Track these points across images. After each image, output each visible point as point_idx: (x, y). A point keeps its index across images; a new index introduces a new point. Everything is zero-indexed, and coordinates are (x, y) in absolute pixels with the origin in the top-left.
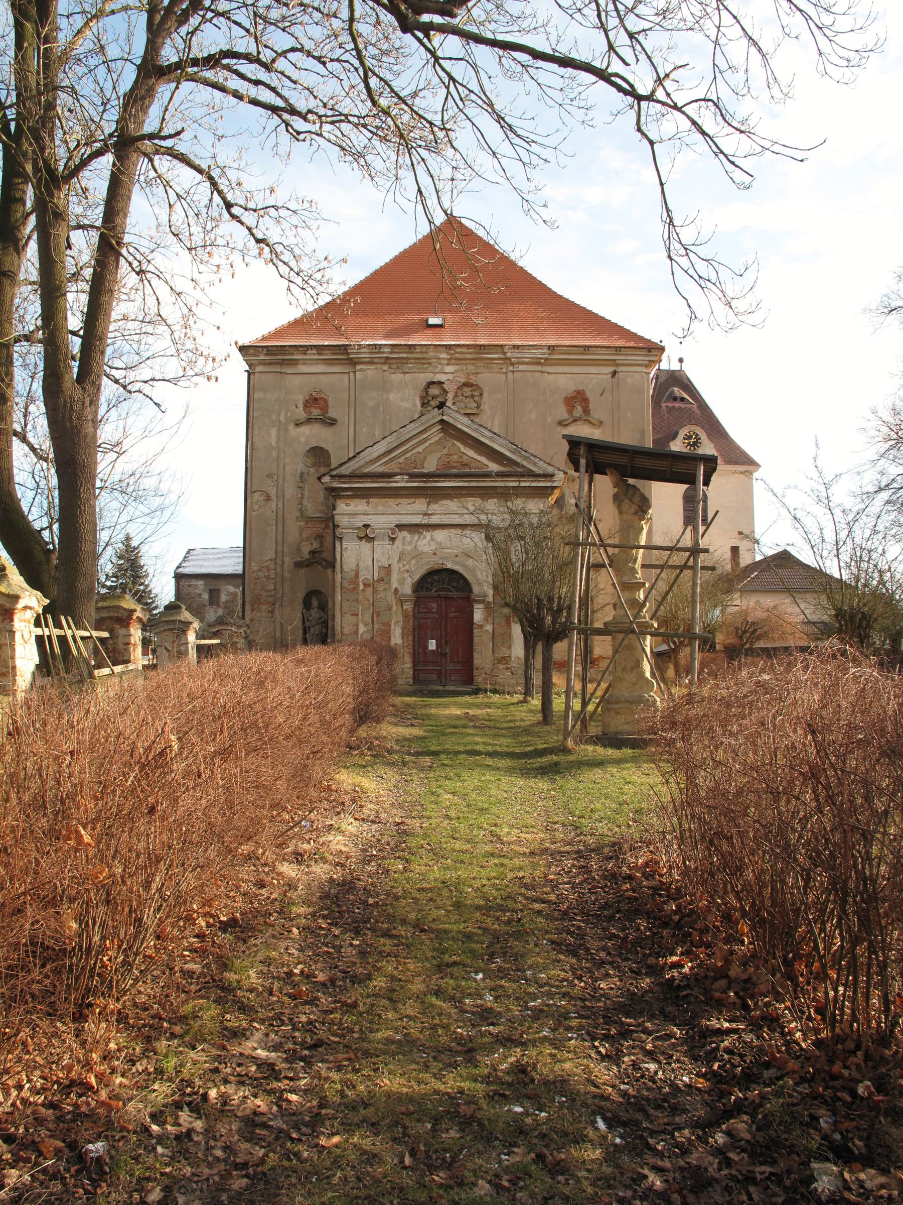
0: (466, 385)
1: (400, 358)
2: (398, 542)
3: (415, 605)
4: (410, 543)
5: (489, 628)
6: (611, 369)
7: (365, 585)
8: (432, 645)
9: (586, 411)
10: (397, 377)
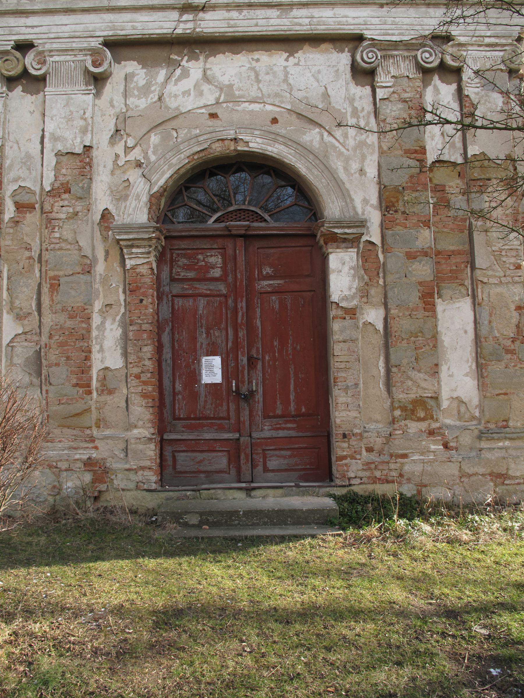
2: (112, 89)
3: (161, 259)
4: (145, 90)
5: (374, 316)
7: (19, 207)
8: (212, 370)
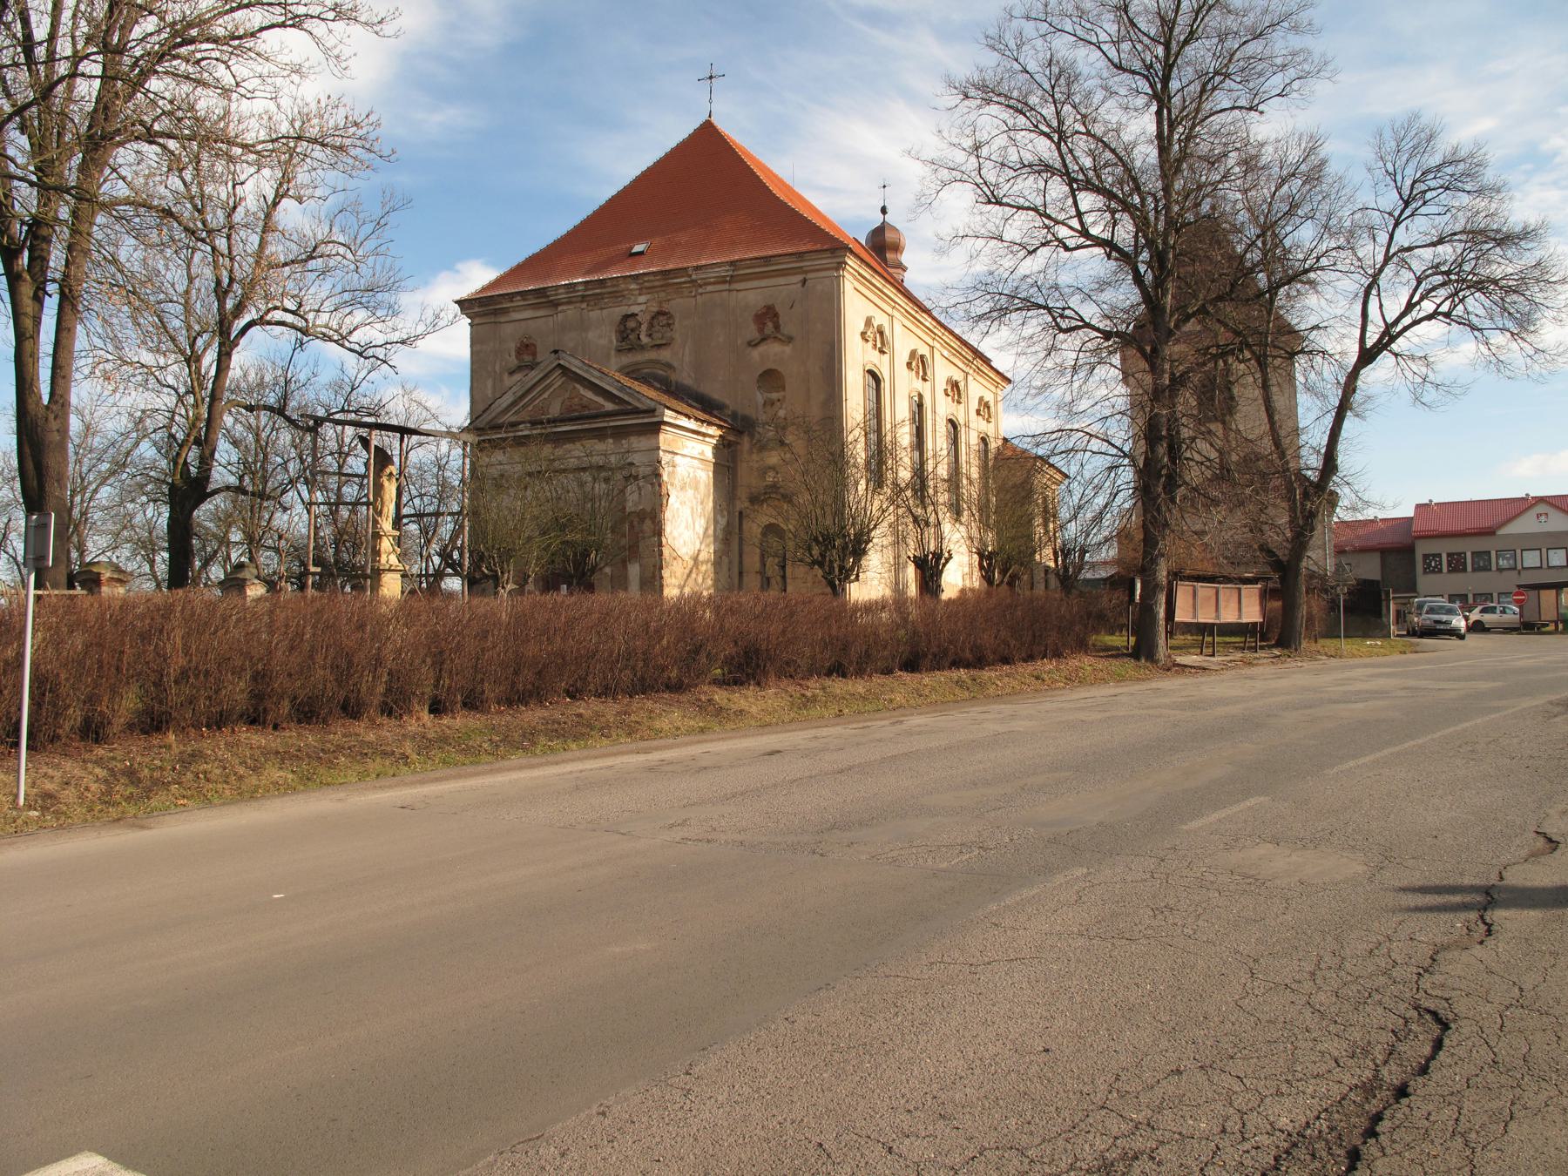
0: (661, 313)
1: (596, 294)
6: (800, 277)
9: (777, 327)
10: (595, 314)
